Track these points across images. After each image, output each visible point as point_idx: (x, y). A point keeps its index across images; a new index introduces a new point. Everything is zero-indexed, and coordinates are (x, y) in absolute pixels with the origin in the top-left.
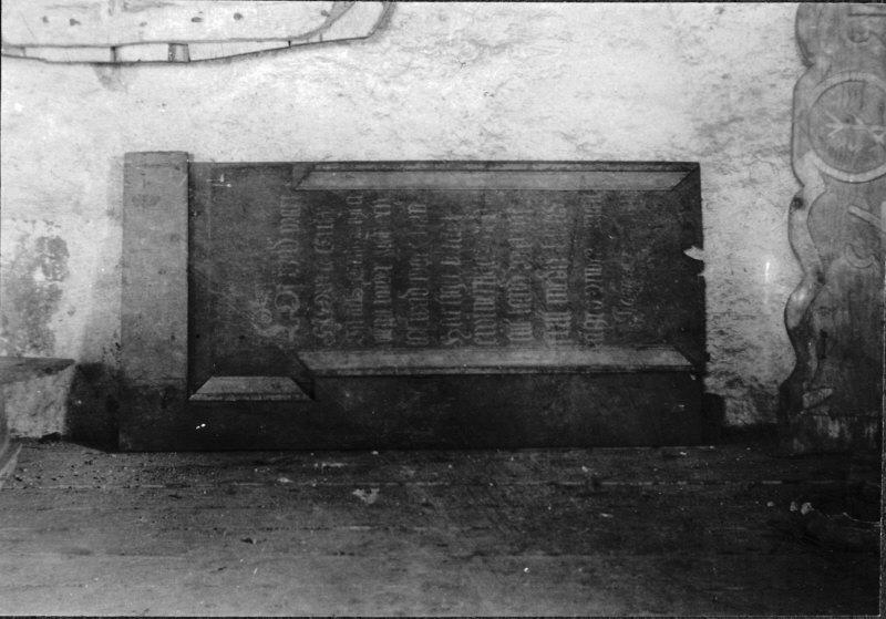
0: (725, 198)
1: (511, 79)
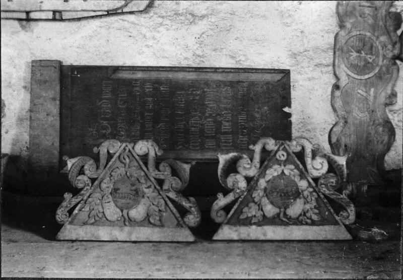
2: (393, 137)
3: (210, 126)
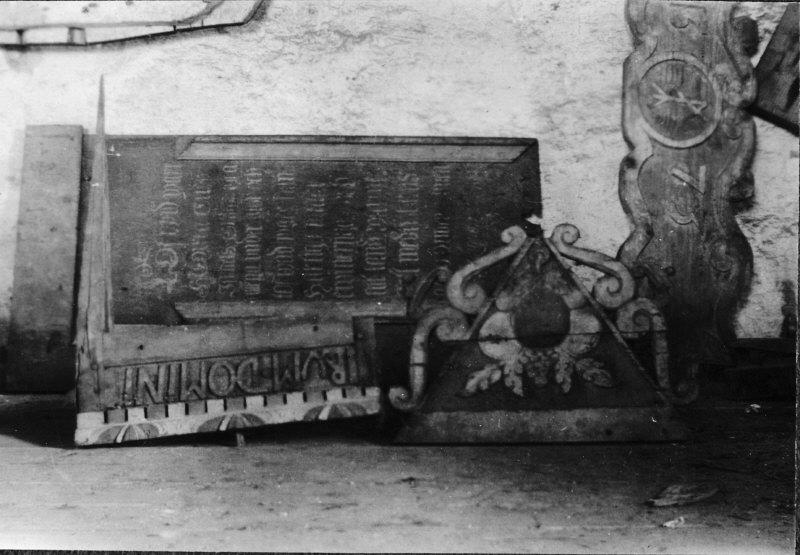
0: (561, 172)
1: (372, 65)
2: (748, 265)
3: (375, 251)
